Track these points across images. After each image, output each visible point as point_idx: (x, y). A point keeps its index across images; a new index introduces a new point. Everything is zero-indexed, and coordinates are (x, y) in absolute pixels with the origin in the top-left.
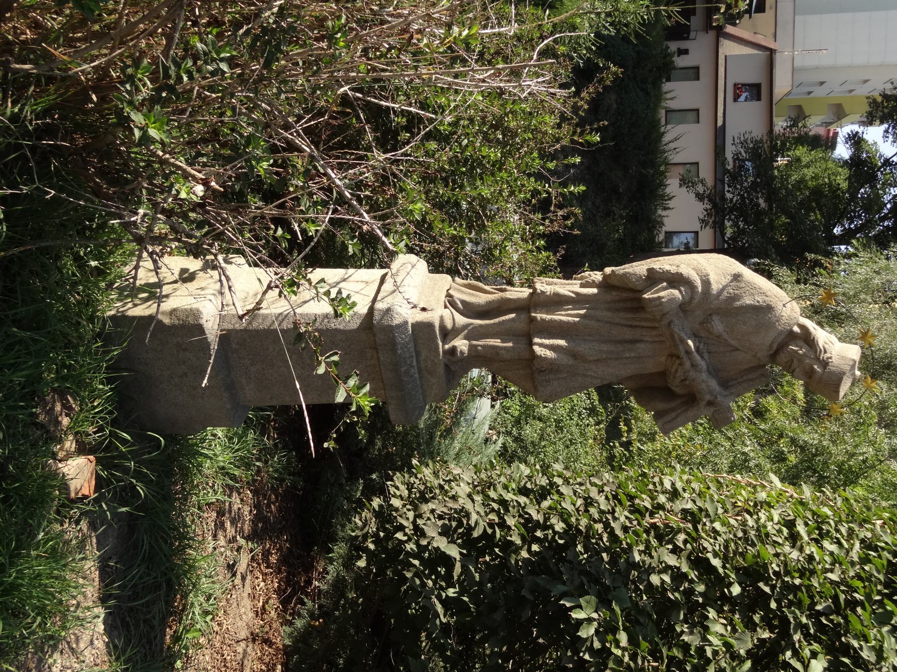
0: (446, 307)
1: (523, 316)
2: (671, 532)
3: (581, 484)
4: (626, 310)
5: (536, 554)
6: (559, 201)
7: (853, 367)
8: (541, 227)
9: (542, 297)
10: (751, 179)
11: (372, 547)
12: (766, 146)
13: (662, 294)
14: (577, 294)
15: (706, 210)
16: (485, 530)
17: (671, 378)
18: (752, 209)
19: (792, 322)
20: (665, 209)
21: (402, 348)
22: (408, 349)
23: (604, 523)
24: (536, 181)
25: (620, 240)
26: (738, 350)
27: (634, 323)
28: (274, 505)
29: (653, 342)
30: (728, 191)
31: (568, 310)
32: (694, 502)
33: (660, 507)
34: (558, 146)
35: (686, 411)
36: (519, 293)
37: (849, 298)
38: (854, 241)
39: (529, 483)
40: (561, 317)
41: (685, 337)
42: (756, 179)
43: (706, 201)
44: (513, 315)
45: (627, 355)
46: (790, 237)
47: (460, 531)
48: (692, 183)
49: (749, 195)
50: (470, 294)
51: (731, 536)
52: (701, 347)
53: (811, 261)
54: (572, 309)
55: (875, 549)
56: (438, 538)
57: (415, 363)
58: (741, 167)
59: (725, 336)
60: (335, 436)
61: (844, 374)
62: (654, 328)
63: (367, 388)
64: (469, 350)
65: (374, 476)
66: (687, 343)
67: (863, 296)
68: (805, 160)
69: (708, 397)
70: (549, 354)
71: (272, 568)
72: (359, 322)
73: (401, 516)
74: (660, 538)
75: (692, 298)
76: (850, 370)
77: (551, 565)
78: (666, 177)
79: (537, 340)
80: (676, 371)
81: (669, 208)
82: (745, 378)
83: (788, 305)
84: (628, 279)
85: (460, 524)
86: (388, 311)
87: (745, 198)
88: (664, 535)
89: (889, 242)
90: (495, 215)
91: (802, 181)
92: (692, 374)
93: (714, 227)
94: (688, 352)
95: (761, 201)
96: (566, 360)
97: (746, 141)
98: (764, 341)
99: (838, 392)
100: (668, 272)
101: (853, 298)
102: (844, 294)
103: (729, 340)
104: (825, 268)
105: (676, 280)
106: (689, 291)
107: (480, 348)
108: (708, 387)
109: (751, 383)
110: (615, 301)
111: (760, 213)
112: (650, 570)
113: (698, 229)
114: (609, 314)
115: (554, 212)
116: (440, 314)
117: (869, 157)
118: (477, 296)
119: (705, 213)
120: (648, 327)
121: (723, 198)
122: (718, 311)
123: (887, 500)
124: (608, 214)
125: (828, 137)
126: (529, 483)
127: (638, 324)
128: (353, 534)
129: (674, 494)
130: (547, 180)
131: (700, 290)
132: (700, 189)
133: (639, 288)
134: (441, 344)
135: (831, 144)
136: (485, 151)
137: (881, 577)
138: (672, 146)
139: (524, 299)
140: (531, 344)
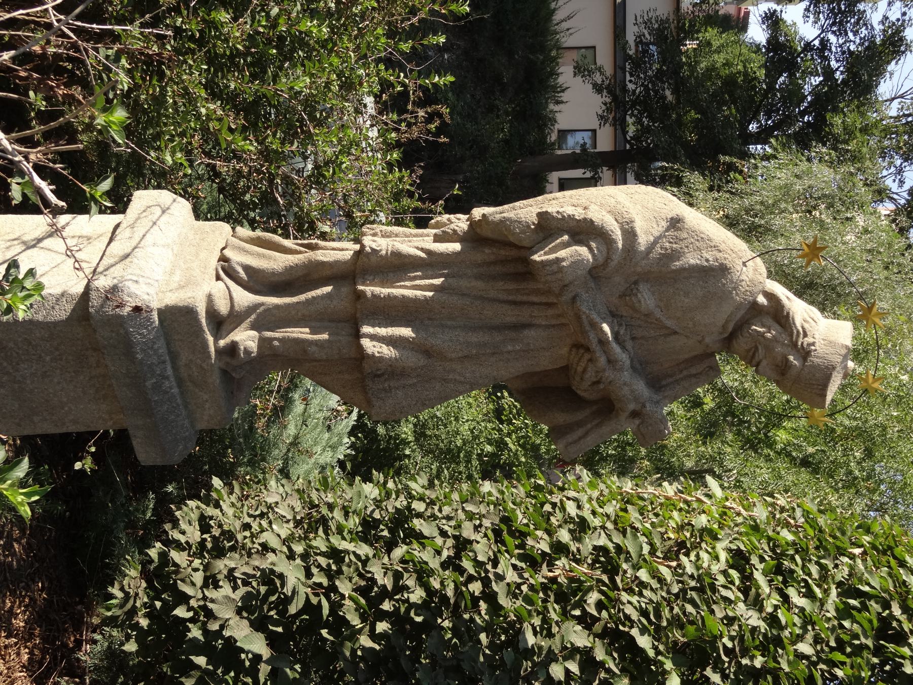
0: (218, 278)
1: (345, 290)
2: (579, 589)
3: (449, 518)
4: (506, 277)
5: (384, 636)
6: (419, 98)
7: (845, 358)
8: (393, 135)
9: (373, 259)
10: (656, 66)
11: (144, 623)
12: (672, 26)
13: (562, 254)
14: (429, 252)
15: (605, 104)
16: (308, 599)
17: (577, 378)
18: (658, 102)
19: (756, 290)
20: (558, 102)
21: (143, 350)
22: (156, 351)
23: (482, 579)
24: (386, 69)
25: (506, 142)
26: (675, 333)
27: (519, 298)
28: (19, 543)
29: (548, 327)
30: (630, 81)
31: (415, 278)
32: (609, 536)
33: (560, 549)
34: (415, 20)
35: (598, 425)
36: (339, 251)
37: (767, 208)
38: (772, 140)
39: (377, 511)
40: (404, 290)
41: (598, 320)
42: (661, 67)
43: (605, 93)
44: (329, 289)
45: (510, 348)
46: (701, 136)
47: (273, 598)
48: (589, 72)
49: (653, 85)
50: (259, 255)
51: (664, 594)
52: (622, 332)
53: (724, 163)
54: (421, 278)
55: (859, 594)
56: (234, 620)
57: (169, 372)
58: (645, 51)
59: (658, 314)
60: (93, 449)
61: (834, 368)
62: (549, 305)
63: (25, 465)
64: (259, 347)
65: (170, 489)
66: (601, 329)
67: (783, 205)
68: (716, 44)
69: (632, 406)
70: (387, 351)
71: (16, 636)
72: (69, 307)
73: (183, 581)
74: (562, 598)
75: (608, 259)
76: (842, 363)
77: (403, 662)
78: (557, 64)
79: (366, 329)
80: (585, 371)
81: (562, 102)
82: (685, 373)
83: (750, 264)
84: (508, 229)
85: (272, 591)
86: (115, 289)
87: (649, 89)
88: (567, 595)
89: (810, 140)
90: (326, 118)
91: (711, 69)
92: (609, 374)
93: (614, 125)
94: (603, 342)
95: (668, 93)
96: (414, 360)
97: (650, 20)
98: (716, 318)
99: (824, 396)
100: (571, 218)
101: (770, 209)
102: (762, 203)
103: (663, 319)
104: (741, 172)
105: (583, 231)
106: (604, 249)
107: (276, 343)
108: (632, 391)
109: (694, 380)
110: (490, 264)
111: (666, 108)
112: (551, 657)
113: (597, 127)
114: (479, 284)
115: (412, 113)
116: (203, 289)
117: (787, 40)
118: (269, 258)
119: (604, 107)
120: (540, 304)
121: (624, 89)
122: (646, 277)
123: (814, 445)
124: (491, 109)
125: (738, 17)
126: (377, 511)
127: (525, 298)
128: (109, 614)
129: (581, 527)
130: (402, 69)
131: (620, 246)
132: (598, 78)
133: (526, 243)
134: (210, 339)
135: (742, 25)
136: (308, 24)
137: (869, 643)
138: (565, 25)
139: (345, 263)
140: (358, 335)
